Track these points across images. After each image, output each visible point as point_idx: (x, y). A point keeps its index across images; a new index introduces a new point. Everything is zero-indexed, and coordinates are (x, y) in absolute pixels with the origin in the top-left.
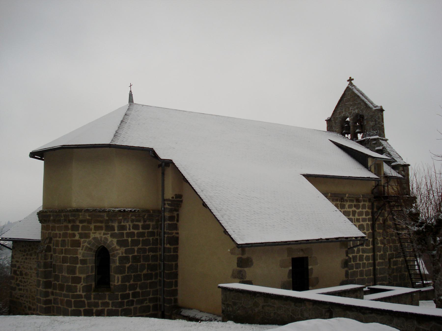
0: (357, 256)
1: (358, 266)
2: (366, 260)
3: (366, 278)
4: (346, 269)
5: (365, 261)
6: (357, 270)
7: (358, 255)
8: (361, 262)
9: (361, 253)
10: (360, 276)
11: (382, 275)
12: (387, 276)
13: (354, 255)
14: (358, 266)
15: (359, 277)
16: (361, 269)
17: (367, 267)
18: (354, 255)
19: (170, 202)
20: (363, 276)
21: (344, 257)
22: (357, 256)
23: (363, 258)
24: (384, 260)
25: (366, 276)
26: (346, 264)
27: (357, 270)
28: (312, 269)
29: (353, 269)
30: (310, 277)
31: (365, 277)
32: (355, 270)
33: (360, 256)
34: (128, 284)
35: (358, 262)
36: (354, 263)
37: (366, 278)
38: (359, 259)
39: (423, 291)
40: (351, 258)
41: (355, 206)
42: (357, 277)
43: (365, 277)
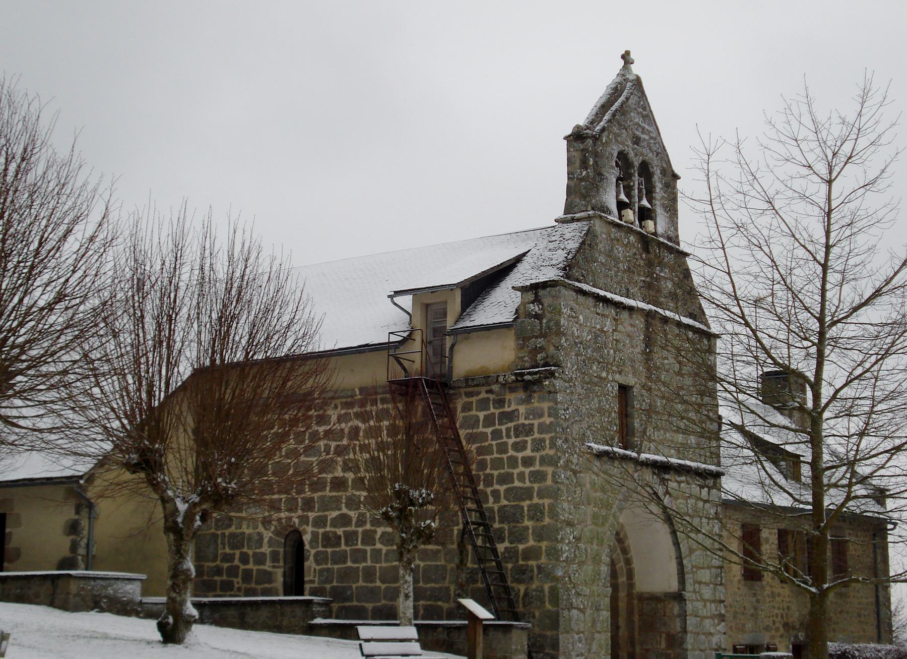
0: (356, 533)
1: (359, 556)
2: (382, 543)
3: (383, 586)
4: (73, 537)
5: (378, 546)
6: (356, 565)
7: (360, 530)
8: (368, 548)
9: (368, 526)
10: (365, 581)
11: (433, 585)
12: (452, 588)
13: (348, 529)
14: (359, 556)
15: (361, 583)
16: (369, 563)
17: (387, 561)
18: (348, 529)
19: (888, 493)
20: (373, 581)
21: (72, 515)
22: (356, 533)
23: (374, 539)
24: (443, 544)
25: (383, 582)
26: (73, 528)
27: (356, 565)
28: (10, 533)
29: (345, 562)
30: (6, 547)
31: (378, 583)
32: (349, 564)
33: (365, 533)
34: (328, 586)
35: (360, 546)
36: (348, 549)
37: (383, 586)
38: (362, 539)
39: (205, 603)
40: (340, 537)
41: (357, 416)
42: (358, 581)
43: (378, 583)
